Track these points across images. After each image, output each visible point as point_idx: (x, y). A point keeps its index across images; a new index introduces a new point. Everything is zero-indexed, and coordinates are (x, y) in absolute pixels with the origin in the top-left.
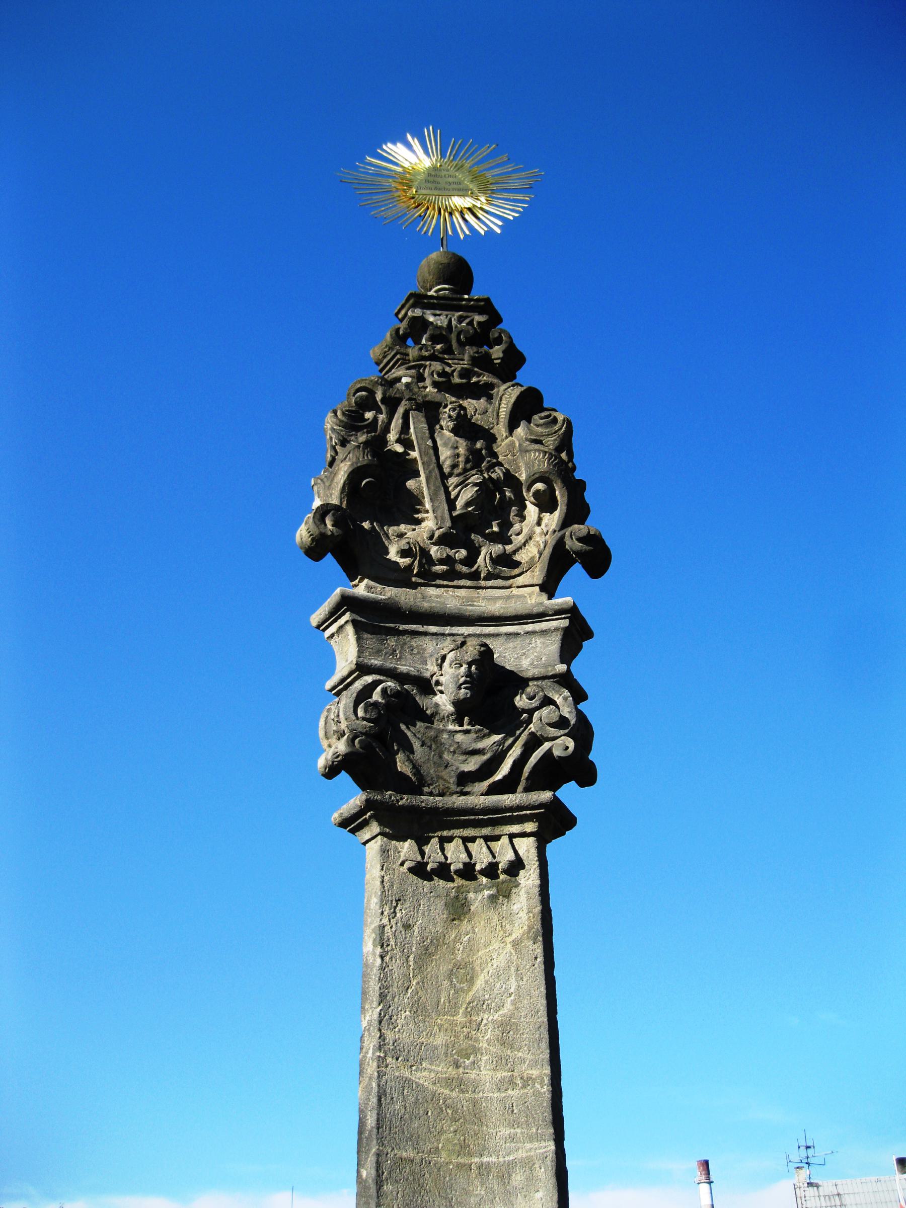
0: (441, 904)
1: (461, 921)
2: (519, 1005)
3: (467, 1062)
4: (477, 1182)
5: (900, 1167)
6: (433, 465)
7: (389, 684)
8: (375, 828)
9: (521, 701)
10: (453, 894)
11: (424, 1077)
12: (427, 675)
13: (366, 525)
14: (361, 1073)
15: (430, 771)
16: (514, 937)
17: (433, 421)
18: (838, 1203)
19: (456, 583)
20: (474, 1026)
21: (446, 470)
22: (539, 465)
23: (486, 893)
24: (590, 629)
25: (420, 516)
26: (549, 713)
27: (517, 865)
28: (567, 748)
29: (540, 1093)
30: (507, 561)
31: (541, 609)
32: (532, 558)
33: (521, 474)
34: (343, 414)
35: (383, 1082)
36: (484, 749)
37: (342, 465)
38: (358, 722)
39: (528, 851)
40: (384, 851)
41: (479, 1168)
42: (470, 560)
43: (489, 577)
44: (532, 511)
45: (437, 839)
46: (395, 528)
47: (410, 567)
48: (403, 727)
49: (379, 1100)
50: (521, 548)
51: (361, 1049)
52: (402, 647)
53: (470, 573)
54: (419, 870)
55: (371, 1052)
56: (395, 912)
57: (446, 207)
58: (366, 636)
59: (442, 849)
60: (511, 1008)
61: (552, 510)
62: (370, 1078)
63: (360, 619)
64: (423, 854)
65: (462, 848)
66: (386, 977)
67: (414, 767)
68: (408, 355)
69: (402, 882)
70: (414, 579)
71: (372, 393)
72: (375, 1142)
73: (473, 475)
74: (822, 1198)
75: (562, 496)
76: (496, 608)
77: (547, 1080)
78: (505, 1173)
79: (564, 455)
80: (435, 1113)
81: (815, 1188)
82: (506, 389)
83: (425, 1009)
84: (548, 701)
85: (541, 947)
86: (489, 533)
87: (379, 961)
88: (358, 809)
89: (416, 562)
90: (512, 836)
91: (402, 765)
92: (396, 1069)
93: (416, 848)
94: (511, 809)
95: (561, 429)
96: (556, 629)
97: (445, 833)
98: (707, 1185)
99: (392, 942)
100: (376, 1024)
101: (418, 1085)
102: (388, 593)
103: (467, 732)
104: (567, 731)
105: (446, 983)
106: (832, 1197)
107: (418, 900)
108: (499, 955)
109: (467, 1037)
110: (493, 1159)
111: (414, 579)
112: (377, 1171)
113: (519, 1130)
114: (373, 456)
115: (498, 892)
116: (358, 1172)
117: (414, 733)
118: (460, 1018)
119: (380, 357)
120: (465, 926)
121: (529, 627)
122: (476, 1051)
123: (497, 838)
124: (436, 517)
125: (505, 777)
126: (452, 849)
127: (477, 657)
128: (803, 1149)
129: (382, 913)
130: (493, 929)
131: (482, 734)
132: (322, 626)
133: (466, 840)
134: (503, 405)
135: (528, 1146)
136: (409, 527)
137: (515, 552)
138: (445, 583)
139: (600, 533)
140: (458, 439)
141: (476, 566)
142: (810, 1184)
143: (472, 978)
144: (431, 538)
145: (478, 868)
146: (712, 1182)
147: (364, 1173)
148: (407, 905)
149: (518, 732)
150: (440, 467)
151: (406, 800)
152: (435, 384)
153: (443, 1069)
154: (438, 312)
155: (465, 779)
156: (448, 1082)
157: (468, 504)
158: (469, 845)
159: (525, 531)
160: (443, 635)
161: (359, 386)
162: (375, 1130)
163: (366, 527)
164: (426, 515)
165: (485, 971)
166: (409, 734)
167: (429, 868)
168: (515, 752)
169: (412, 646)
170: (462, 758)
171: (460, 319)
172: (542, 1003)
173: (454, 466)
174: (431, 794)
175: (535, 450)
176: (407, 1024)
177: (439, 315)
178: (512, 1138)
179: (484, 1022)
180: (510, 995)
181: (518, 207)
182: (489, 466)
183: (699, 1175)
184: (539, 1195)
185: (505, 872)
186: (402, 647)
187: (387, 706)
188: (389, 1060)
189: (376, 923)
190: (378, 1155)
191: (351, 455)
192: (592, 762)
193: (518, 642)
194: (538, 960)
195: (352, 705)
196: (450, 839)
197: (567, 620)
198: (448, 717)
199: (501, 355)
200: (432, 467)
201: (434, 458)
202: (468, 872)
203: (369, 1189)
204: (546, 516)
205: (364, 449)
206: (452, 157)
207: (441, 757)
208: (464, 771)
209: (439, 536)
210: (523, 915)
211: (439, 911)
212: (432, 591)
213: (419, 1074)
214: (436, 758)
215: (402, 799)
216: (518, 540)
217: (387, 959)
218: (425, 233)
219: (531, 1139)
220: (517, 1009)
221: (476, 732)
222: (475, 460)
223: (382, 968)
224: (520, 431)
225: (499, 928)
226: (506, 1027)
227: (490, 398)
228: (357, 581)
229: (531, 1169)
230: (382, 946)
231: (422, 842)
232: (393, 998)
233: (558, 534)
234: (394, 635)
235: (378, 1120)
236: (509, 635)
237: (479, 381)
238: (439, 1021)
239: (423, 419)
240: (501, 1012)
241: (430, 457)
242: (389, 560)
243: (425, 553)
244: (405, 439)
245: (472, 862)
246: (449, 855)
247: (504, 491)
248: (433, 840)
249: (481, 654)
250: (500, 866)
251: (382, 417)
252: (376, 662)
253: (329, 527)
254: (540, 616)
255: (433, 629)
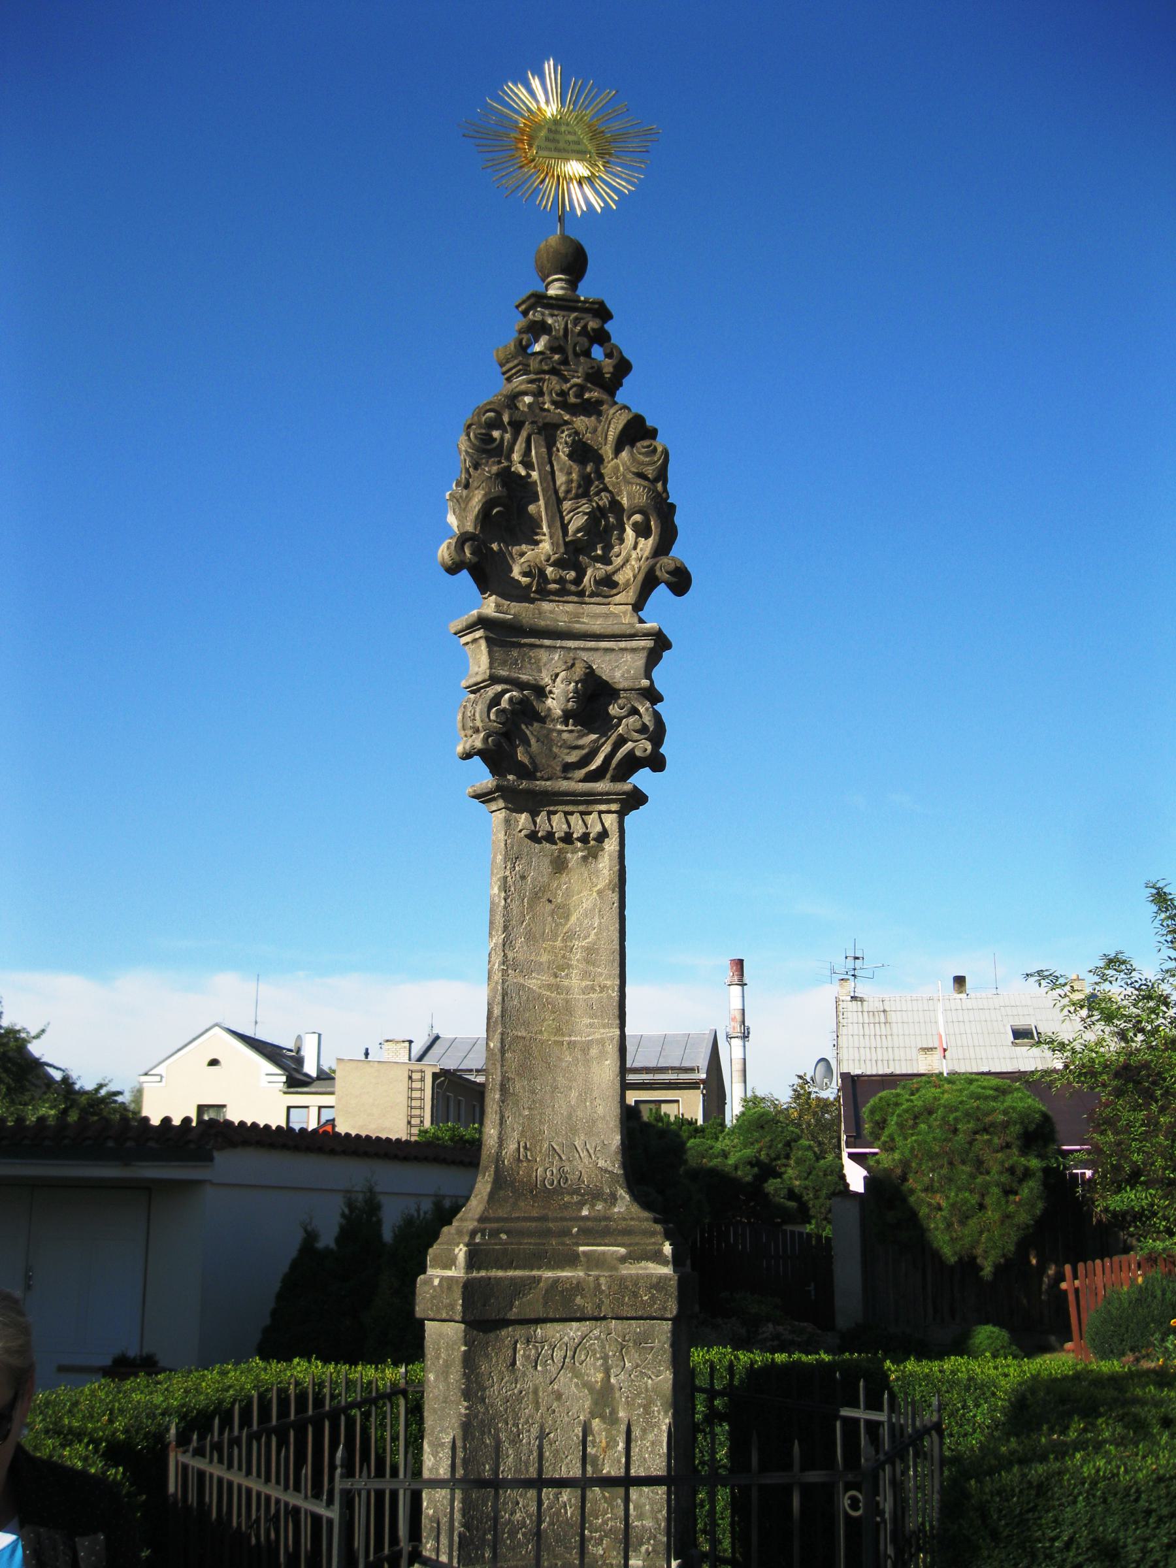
0: (547, 861)
1: (562, 874)
2: (600, 936)
3: (563, 974)
4: (567, 1053)
5: (956, 986)
6: (551, 492)
7: (514, 693)
8: (501, 803)
9: (614, 710)
10: (556, 855)
11: (533, 983)
12: (542, 683)
13: (495, 546)
14: (489, 978)
15: (542, 760)
16: (599, 887)
17: (550, 444)
18: (883, 1020)
19: (565, 598)
20: (568, 949)
21: (561, 495)
22: (639, 499)
23: (580, 854)
24: (669, 640)
25: (538, 538)
26: (634, 722)
27: (603, 835)
28: (646, 750)
29: (612, 997)
30: (608, 583)
31: (633, 631)
32: (628, 580)
33: (622, 498)
34: (476, 437)
35: (505, 987)
36: (583, 745)
37: (476, 492)
38: (490, 724)
39: (612, 824)
40: (507, 821)
41: (568, 1044)
42: (578, 581)
43: (592, 595)
44: (630, 533)
45: (545, 813)
46: (518, 547)
47: (529, 586)
48: (523, 727)
49: (503, 999)
50: (619, 569)
51: (489, 962)
52: (523, 657)
53: (577, 592)
54: (533, 836)
55: (497, 965)
56: (514, 867)
57: (565, 175)
58: (496, 649)
59: (549, 820)
60: (595, 937)
61: (646, 538)
62: (497, 983)
63: (491, 635)
64: (535, 823)
65: (563, 820)
66: (508, 913)
67: (531, 757)
68: (529, 366)
69: (520, 844)
70: (532, 595)
71: (499, 415)
72: (500, 1026)
73: (584, 504)
74: (865, 1014)
75: (656, 528)
76: (597, 626)
77: (616, 988)
78: (586, 1048)
79: (659, 486)
80: (540, 1007)
81: (859, 1003)
82: (615, 413)
83: (535, 937)
84: (634, 711)
85: (618, 896)
86: (594, 556)
87: (503, 902)
88: (489, 790)
89: (535, 582)
90: (600, 813)
91: (521, 755)
92: (514, 978)
93: (531, 819)
94: (601, 794)
95: (659, 460)
96: (643, 648)
97: (551, 808)
98: (739, 988)
99: (513, 889)
100: (501, 946)
101: (529, 988)
102: (516, 610)
103: (571, 731)
104: (646, 736)
105: (550, 919)
106: (876, 1013)
107: (531, 858)
108: (587, 899)
109: (564, 957)
110: (578, 1038)
111: (532, 595)
112: (502, 1044)
113: (596, 1021)
114: (503, 487)
115: (589, 853)
116: (487, 1044)
117: (531, 731)
118: (559, 943)
119: (504, 361)
120: (564, 878)
121: (623, 645)
122: (569, 966)
123: (590, 813)
124: (552, 543)
125: (598, 768)
126: (557, 820)
127: (583, 677)
128: (850, 961)
129: (506, 868)
130: (584, 882)
131: (581, 734)
132: (460, 633)
133: (566, 814)
134: (611, 429)
135: (602, 1031)
136: (530, 547)
137: (615, 573)
138: (557, 598)
139: (682, 563)
140: (572, 463)
141: (583, 585)
142: (854, 998)
143: (568, 916)
144: (548, 560)
145: (575, 836)
146: (746, 984)
147: (492, 1045)
148: (523, 862)
149: (610, 734)
150: (556, 492)
151: (524, 784)
152: (553, 403)
153: (546, 978)
154: (556, 312)
155: (568, 768)
156: (550, 987)
157: (578, 530)
158: (569, 817)
159: (624, 554)
160: (555, 647)
161: (488, 407)
162: (500, 1018)
163: (495, 549)
164: (543, 538)
165: (577, 911)
166: (528, 732)
167: (540, 835)
168: (606, 749)
169: (530, 656)
170: (566, 751)
171: (576, 321)
172: (616, 936)
173: (568, 491)
174: (542, 779)
175: (639, 484)
176: (523, 947)
177: (557, 316)
178: (591, 1025)
179: (576, 946)
180: (595, 928)
181: (634, 177)
182: (597, 491)
183: (729, 974)
184: (607, 1062)
185: (594, 839)
186: (523, 657)
187: (513, 712)
188: (510, 971)
189: (501, 875)
190: (502, 1034)
191: (484, 484)
192: (663, 756)
193: (612, 656)
194: (615, 905)
195: (486, 710)
196: (555, 813)
197: (653, 641)
198: (557, 719)
199: (611, 370)
200: (550, 493)
201: (551, 483)
202: (568, 839)
203: (496, 1055)
204: (642, 540)
205: (495, 479)
206: (572, 107)
207: (551, 750)
208: (567, 762)
209: (554, 561)
210: (606, 872)
211: (546, 867)
212: (546, 606)
213: (530, 981)
214: (547, 752)
215: (522, 783)
216: (618, 561)
217: (509, 901)
218: (544, 208)
219: (604, 1026)
220: (599, 939)
221: (578, 732)
222: (584, 489)
223: (505, 907)
224: (624, 454)
225: (588, 880)
226: (590, 950)
227: (599, 414)
228: (487, 595)
229: (603, 1045)
230: (505, 892)
231: (534, 814)
232: (513, 929)
233: (651, 562)
234: (517, 647)
235: (502, 1011)
236: (606, 650)
237: (592, 398)
238: (544, 945)
239: (543, 443)
240: (587, 941)
241: (548, 483)
242: (513, 578)
243: (542, 573)
244: (526, 462)
245: (571, 831)
246: (554, 825)
247: (608, 517)
248: (542, 813)
249: (586, 674)
250: (591, 835)
251: (507, 436)
252: (503, 673)
253: (468, 555)
254: (632, 636)
255: (547, 642)
